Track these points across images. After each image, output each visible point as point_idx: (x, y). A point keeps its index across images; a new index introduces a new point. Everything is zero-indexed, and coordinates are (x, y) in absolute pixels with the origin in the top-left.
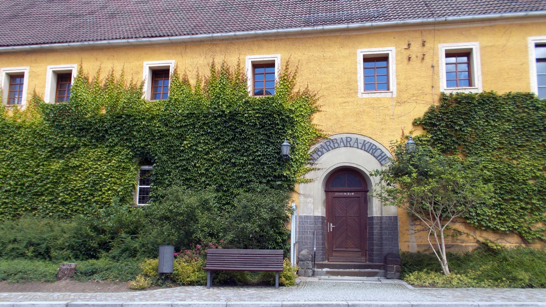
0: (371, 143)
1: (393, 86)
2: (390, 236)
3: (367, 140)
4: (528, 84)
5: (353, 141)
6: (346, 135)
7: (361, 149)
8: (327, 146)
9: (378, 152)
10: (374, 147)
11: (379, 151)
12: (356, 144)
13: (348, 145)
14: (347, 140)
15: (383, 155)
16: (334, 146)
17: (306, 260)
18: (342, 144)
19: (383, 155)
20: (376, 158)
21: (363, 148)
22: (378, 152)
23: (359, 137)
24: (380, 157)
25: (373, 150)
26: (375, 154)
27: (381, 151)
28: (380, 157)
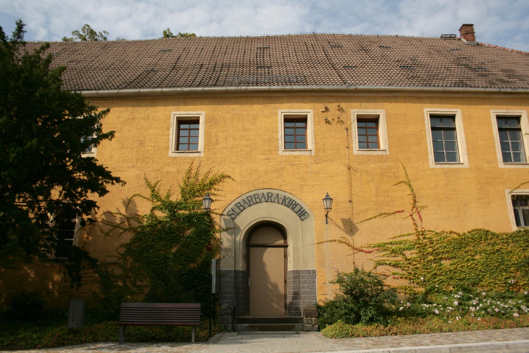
1: (310, 144)
3: (288, 195)
5: (274, 196)
6: (265, 192)
7: (282, 204)
8: (249, 201)
9: (298, 208)
10: (294, 203)
12: (277, 199)
13: (270, 200)
14: (268, 196)
15: (302, 210)
16: (256, 201)
18: (246, 205)
19: (302, 210)
20: (296, 213)
21: (284, 204)
22: (298, 208)
23: (269, 191)
24: (300, 212)
25: (293, 205)
28: (300, 212)
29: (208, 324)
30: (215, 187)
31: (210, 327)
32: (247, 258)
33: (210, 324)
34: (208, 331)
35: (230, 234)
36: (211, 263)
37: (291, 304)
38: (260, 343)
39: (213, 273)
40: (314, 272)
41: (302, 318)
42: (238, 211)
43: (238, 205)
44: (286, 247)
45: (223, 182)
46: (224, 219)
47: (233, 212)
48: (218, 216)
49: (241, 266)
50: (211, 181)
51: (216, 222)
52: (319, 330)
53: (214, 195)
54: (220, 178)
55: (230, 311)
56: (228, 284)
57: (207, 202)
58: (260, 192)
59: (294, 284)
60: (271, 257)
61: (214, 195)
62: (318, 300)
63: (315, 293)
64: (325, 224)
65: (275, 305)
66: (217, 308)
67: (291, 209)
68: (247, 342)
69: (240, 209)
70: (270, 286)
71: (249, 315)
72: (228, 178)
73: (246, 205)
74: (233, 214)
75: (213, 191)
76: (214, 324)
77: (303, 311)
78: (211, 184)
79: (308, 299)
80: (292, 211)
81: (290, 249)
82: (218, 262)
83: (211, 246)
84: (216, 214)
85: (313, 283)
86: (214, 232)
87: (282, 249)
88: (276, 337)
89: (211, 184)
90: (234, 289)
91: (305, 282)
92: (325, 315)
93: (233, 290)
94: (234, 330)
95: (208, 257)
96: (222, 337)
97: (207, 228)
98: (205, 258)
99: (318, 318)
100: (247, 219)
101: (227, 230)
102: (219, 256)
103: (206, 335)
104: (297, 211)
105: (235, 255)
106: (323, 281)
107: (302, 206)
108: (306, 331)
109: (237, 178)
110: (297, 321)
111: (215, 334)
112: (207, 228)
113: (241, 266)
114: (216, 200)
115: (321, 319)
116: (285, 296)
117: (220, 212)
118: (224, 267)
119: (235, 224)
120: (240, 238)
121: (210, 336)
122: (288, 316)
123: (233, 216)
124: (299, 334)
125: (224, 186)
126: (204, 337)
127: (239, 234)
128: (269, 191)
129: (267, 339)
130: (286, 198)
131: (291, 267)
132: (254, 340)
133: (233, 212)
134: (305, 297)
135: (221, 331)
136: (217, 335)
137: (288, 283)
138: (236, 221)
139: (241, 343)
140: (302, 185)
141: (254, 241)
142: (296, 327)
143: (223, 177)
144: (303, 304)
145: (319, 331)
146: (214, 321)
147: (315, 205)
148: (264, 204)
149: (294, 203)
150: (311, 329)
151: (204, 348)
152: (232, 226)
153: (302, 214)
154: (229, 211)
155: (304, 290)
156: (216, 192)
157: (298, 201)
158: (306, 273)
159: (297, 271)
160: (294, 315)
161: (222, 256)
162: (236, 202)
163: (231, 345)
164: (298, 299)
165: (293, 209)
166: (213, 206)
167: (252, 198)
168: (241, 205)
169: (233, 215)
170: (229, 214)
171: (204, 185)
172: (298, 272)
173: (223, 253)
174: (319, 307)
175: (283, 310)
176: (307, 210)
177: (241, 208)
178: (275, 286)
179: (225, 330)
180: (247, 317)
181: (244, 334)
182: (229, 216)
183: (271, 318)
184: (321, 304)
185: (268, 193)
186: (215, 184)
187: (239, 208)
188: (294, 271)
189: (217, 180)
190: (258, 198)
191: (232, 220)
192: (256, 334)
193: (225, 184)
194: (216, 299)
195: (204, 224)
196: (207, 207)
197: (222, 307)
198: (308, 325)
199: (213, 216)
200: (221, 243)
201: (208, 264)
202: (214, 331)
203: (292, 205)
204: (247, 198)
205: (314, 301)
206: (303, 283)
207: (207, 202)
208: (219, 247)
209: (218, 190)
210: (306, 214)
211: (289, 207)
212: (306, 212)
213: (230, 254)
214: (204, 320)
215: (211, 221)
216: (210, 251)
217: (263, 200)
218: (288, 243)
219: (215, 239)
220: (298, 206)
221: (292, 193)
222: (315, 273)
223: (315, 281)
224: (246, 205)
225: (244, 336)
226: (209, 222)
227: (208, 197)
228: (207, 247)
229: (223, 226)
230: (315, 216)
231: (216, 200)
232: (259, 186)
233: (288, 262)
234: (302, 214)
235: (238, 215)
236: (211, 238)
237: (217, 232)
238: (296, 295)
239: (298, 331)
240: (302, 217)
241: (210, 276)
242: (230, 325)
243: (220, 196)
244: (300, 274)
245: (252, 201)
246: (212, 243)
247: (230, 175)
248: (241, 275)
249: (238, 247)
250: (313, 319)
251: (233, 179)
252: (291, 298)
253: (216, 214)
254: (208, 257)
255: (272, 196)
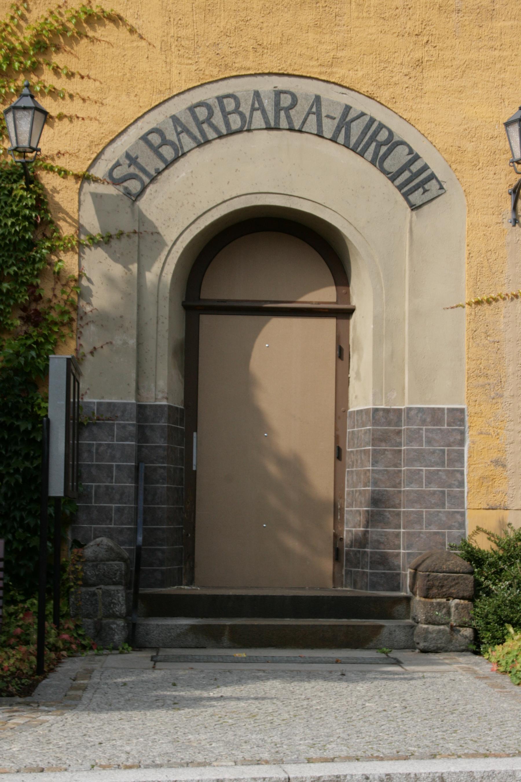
0: (372, 120)
2: (434, 488)
3: (359, 104)
4: (338, 103)
5: (303, 106)
6: (266, 86)
7: (334, 140)
8: (199, 124)
9: (400, 156)
10: (383, 136)
11: (401, 150)
12: (313, 118)
13: (284, 124)
14: (277, 103)
15: (415, 168)
16: (227, 124)
17: (106, 579)
18: (187, 142)
19: (415, 168)
20: (393, 179)
21: (341, 139)
22: (400, 156)
23: (283, 83)
24: (406, 175)
25: (380, 145)
26: (387, 164)
27: (411, 151)
28: (406, 175)
29: (32, 620)
30: (58, 59)
31: (42, 632)
32: (188, 355)
33: (42, 617)
34: (33, 648)
35: (121, 258)
36: (45, 372)
37: (362, 541)
38: (253, 706)
39: (56, 412)
40: (458, 416)
41: (408, 599)
42: (152, 164)
43: (155, 139)
44: (346, 313)
45: (93, 40)
46: (96, 197)
47: (133, 170)
48: (72, 184)
49: (163, 388)
50: (38, 35)
51: (60, 209)
52: (476, 647)
53: (54, 93)
54: (78, 24)
55: (119, 566)
56: (113, 458)
57: (25, 122)
58: (243, 88)
59: (375, 463)
60: (281, 357)
61: (54, 93)
62: (469, 530)
63: (459, 500)
64: (507, 225)
65: (293, 544)
66: (67, 555)
67: (373, 162)
68: (197, 701)
69: (161, 157)
70: (273, 469)
71: (191, 582)
72: (110, 26)
73: (186, 140)
74: (132, 177)
75: (48, 78)
76: (57, 622)
77: (409, 572)
78: (42, 46)
79: (429, 524)
80: (375, 172)
81: (362, 326)
82: (73, 367)
83: (40, 307)
84: (64, 173)
85: (451, 462)
86: (52, 250)
87: (331, 323)
88: (310, 676)
89: (42, 46)
90: (137, 480)
91: (419, 457)
92: (501, 589)
93: (130, 485)
94: (135, 642)
95: (30, 347)
96: (89, 673)
97: (25, 230)
98: (18, 354)
99: (471, 599)
100: (189, 200)
101: (106, 241)
102: (73, 344)
103: (25, 668)
104: (394, 169)
105: (139, 344)
106: (495, 456)
107: (417, 149)
108: (424, 651)
109: (151, 25)
110: (385, 608)
111: (59, 661)
112: (25, 230)
113: (163, 388)
114: (61, 117)
115: (485, 605)
116: (337, 510)
117: (78, 167)
118: (94, 394)
119: (142, 219)
120: (163, 271)
121: (42, 670)
122: (346, 590)
123: (134, 186)
124: (398, 663)
125: (94, 59)
126: (17, 674)
127: (154, 259)
128: (283, 83)
129: (277, 684)
130: (352, 115)
131: (362, 397)
132: (226, 691)
133: (133, 170)
134: (420, 514)
135: (84, 647)
136: (71, 666)
137: (348, 459)
138: (143, 204)
139: (176, 704)
140: (419, 63)
141: (214, 290)
142: (385, 631)
143: (93, 19)
144: (407, 547)
145: (477, 653)
146: (56, 607)
147: (470, 146)
148: (262, 140)
149: (383, 136)
150: (440, 644)
151: (21, 728)
152: (126, 224)
153: (416, 183)
154: (118, 164)
155: (415, 488)
156: (60, 83)
157: (401, 130)
158: (423, 422)
159: (387, 411)
160: (374, 586)
161: (86, 349)
162: (144, 127)
163: (137, 715)
164: (387, 524)
165: (378, 161)
166: (50, 141)
167: (211, 114)
168: (165, 142)
169: (135, 178)
170: (117, 174)
171: (13, 49)
172: (391, 416)
173: (91, 336)
174: (475, 558)
175: (327, 565)
176: (437, 166)
177: (168, 152)
178: (294, 467)
179: (99, 641)
180: (186, 589)
181: (179, 659)
182: (116, 182)
183: (283, 598)
184: (483, 544)
185: (278, 93)
186: (58, 49)
187: (156, 150)
188: (376, 410)
189: (66, 29)
190: (236, 111)
191: (127, 202)
192: (223, 660)
193: (98, 49)
194: (59, 519)
195: (14, 214)
196: (24, 143)
197: (89, 552)
198: (431, 627)
199: (49, 180)
200: (84, 294)
201: (31, 377)
202: (55, 648)
203: (374, 143)
204: (192, 109)
205: (455, 532)
206: (410, 462)
207: (25, 122)
208: (76, 308)
209: (70, 75)
210: (433, 185)
211: (362, 154)
212: (432, 177)
213: (118, 341)
214: (14, 602)
215: (42, 202)
216: (36, 325)
217: (258, 120)
218: (355, 301)
219: (58, 276)
220: (400, 148)
221: (377, 94)
222: (462, 421)
223: (461, 454)
224: (187, 142)
225: (182, 671)
226: (32, 208)
227: (27, 102)
228: (24, 309)
229: (92, 223)
230: (467, 194)
231: (61, 117)
232: (240, 62)
233: (352, 374)
234: (416, 183)
235: (153, 180)
236: (40, 274)
237: (66, 250)
238: (380, 506)
239: (392, 648)
240: (416, 197)
241: (43, 425)
242: (121, 623)
243: (78, 101)
244: (398, 423)
245: (212, 122)
246: (47, 293)
247: (119, 10)
248: (163, 423)
249: (150, 311)
250: (453, 603)
251: (132, 31)
252: (362, 519)
253: (64, 173)
254: (30, 347)
255: (293, 105)
